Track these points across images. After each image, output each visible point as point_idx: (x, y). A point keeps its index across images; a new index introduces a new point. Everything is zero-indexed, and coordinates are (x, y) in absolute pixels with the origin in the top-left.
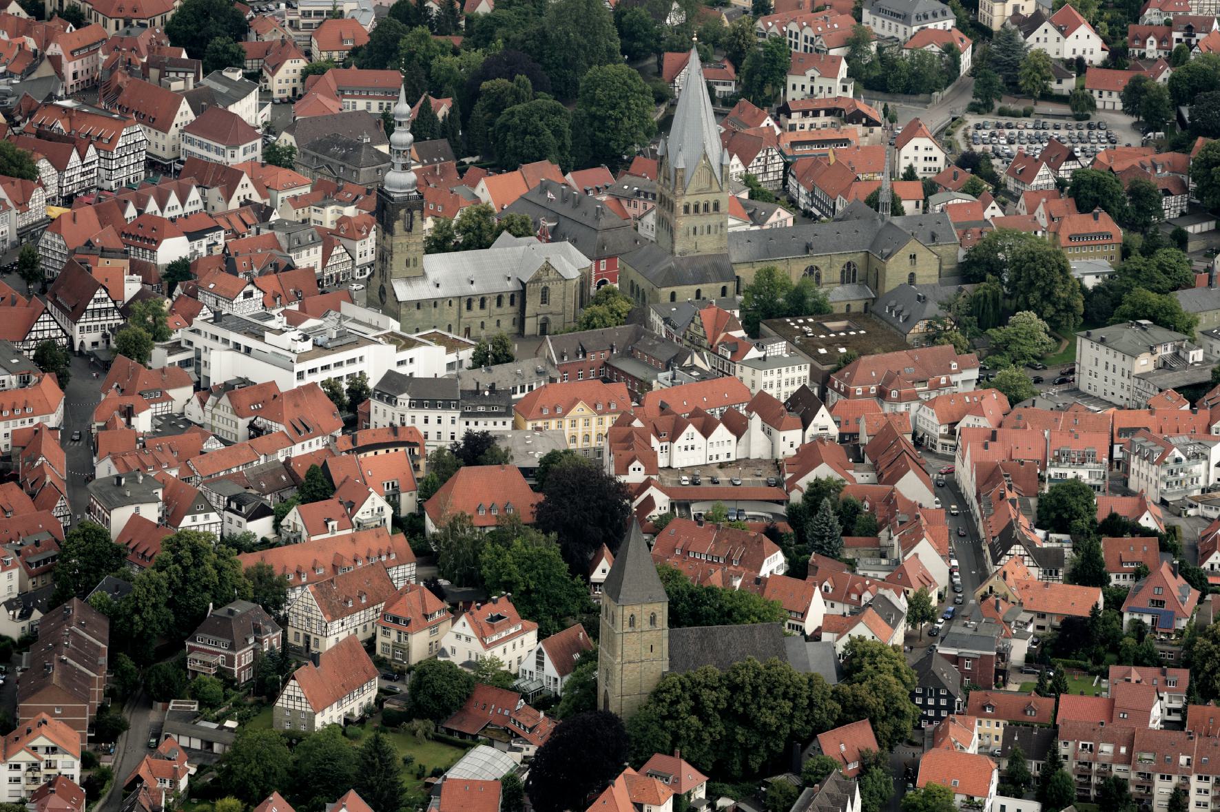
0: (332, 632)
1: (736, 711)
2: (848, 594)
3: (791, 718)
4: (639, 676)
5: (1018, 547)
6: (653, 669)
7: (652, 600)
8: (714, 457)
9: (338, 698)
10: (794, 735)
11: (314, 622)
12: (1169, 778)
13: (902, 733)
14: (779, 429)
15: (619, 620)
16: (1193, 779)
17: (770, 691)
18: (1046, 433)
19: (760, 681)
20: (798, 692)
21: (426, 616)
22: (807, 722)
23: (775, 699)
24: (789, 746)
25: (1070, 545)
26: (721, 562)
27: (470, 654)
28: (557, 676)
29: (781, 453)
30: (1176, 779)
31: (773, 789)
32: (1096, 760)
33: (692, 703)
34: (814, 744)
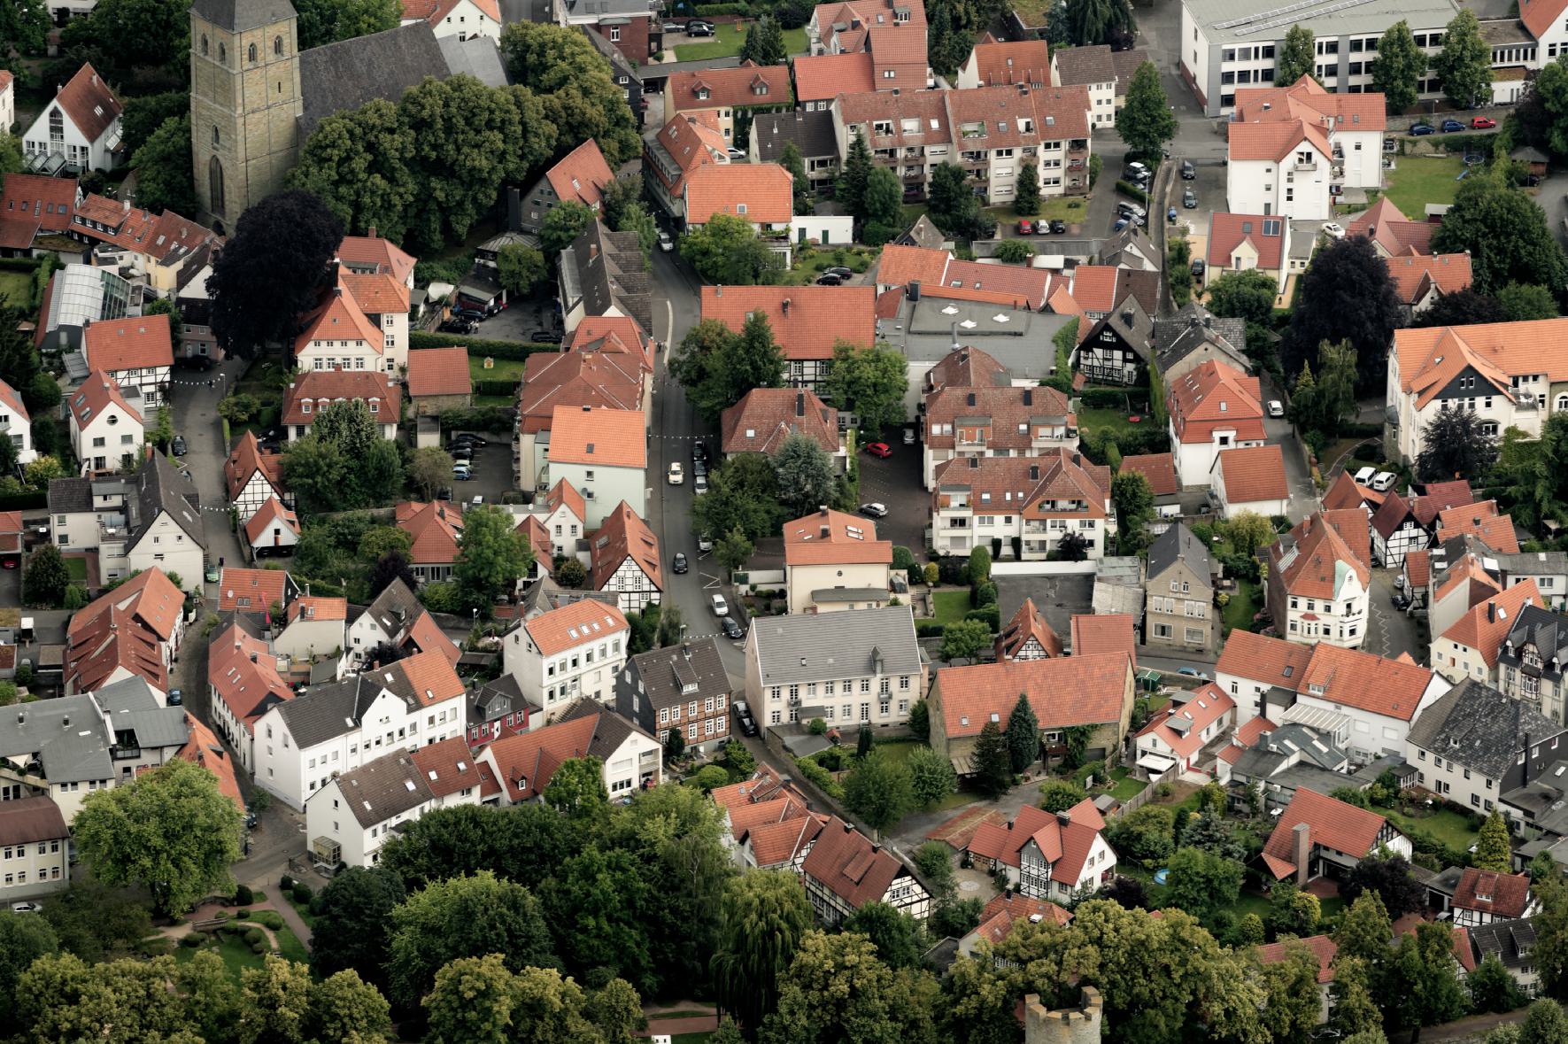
1: (426, 158)
3: (502, 157)
6: (284, 116)
7: (276, 18)
10: (508, 181)
12: (1009, 153)
16: (1041, 149)
17: (468, 122)
22: (522, 157)
23: (478, 132)
28: (85, 143)
30: (1018, 153)
31: (506, 258)
32: (901, 143)
33: (370, 157)
34: (542, 185)
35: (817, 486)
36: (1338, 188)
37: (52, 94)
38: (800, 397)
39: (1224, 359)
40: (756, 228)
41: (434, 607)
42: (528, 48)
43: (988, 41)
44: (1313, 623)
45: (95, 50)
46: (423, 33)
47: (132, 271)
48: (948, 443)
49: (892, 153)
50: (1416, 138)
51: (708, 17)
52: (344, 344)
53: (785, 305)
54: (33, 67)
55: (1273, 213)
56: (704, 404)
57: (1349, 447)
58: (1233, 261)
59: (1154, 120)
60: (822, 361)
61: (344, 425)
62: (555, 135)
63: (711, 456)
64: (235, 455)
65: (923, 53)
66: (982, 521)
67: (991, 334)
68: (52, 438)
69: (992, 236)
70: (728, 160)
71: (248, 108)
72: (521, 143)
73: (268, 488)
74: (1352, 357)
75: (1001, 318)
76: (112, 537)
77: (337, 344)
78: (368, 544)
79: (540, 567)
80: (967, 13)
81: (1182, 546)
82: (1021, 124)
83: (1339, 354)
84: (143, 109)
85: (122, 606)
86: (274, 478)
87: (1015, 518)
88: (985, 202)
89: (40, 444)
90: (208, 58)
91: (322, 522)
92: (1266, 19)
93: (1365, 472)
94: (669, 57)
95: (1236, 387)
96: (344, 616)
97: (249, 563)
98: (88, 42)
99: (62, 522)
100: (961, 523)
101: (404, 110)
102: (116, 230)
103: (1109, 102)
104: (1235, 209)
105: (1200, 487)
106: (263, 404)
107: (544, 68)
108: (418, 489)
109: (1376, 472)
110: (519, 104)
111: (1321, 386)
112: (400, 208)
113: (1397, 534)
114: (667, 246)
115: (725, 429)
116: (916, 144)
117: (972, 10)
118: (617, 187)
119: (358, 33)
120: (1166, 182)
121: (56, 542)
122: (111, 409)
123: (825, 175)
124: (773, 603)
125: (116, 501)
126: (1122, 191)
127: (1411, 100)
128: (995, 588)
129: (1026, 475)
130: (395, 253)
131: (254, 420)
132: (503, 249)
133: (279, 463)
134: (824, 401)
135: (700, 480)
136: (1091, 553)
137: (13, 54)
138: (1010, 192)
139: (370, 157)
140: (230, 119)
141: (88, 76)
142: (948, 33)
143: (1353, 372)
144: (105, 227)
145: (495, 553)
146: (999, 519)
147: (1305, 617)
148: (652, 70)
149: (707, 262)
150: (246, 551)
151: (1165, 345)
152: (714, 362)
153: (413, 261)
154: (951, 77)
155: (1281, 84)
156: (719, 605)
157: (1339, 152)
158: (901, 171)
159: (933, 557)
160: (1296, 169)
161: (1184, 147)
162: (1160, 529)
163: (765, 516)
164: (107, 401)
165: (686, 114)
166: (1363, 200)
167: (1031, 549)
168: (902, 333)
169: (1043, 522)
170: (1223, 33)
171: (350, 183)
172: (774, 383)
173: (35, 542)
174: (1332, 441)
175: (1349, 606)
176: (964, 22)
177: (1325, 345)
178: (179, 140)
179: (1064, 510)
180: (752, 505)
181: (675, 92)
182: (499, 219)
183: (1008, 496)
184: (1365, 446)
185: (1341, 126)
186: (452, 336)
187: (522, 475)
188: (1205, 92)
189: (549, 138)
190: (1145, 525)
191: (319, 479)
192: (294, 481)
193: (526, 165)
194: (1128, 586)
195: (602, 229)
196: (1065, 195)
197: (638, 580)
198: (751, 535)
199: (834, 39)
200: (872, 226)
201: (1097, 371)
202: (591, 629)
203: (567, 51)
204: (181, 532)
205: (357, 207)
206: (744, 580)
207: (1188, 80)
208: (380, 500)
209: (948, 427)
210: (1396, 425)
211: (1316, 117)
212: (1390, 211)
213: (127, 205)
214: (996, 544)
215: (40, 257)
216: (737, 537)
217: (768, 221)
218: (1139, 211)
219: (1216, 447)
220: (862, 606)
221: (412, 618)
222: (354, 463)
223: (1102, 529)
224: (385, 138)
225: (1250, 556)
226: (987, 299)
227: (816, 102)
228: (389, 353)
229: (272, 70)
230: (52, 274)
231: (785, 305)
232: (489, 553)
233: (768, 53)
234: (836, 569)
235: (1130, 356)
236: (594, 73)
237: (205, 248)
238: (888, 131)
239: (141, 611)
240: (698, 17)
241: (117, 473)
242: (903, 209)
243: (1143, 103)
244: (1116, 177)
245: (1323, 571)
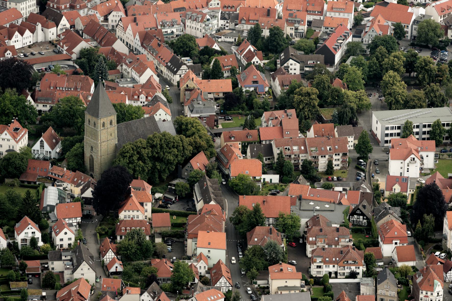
1: (155, 156)
3: (177, 156)
4: (107, 147)
5: (184, 66)
6: (112, 143)
7: (111, 114)
8: (25, 44)
10: (178, 163)
12: (325, 156)
14: (48, 28)
16: (334, 156)
17: (167, 146)
18: (155, 15)
22: (183, 156)
23: (170, 149)
24: (177, 166)
25: (192, 61)
26: (72, 89)
27: (9, 147)
28: (50, 150)
29: (49, 38)
30: (327, 157)
31: (178, 186)
33: (138, 156)
34: (189, 165)
35: (277, 255)
36: (422, 168)
37: (40, 136)
38: (271, 229)
39: (395, 219)
40: (251, 178)
41: (165, 290)
42: (182, 124)
43: (316, 123)
44: (427, 298)
45: (52, 123)
46: (152, 118)
47: (66, 189)
48: (314, 243)
49: (290, 156)
50: (442, 154)
51: (231, 115)
52: (133, 211)
53: (264, 202)
54: (32, 127)
55: (402, 175)
56: (241, 230)
57: (433, 245)
58: (393, 190)
59: (366, 147)
60: (275, 218)
61: (136, 236)
62: (192, 150)
63: (243, 245)
64: (103, 244)
65: (298, 128)
66: (326, 266)
67: (324, 211)
68: (47, 238)
69: (320, 181)
70: (242, 158)
71: (102, 141)
72: (182, 152)
73: (113, 254)
74: (433, 219)
75: (327, 206)
76: (68, 269)
77: (131, 211)
78: (144, 271)
79: (196, 279)
80: (308, 115)
81: (388, 275)
82: (328, 148)
83: (429, 218)
84: (68, 141)
85: (73, 289)
86: (115, 251)
87: (336, 266)
88: (318, 171)
89: (43, 240)
90: (90, 126)
91: (129, 264)
92: (398, 118)
93: (438, 253)
94: (220, 127)
95: (399, 228)
96: (140, 293)
97: (108, 276)
98: (50, 120)
99: (52, 263)
100: (319, 267)
101: (148, 142)
102: (62, 176)
103: (352, 142)
104: (391, 174)
105: (389, 257)
106: (109, 229)
107: (187, 130)
108: (158, 255)
109: (441, 253)
110: (182, 141)
111: (424, 228)
112: (147, 171)
113: (449, 272)
114: (224, 183)
115: (248, 238)
116: (297, 154)
117: (310, 114)
118: (210, 166)
119: (132, 119)
120: (370, 166)
121: (51, 269)
122: (65, 230)
123: (270, 162)
124: (265, 290)
125: (69, 258)
126: (357, 168)
127: (441, 142)
128: (331, 286)
129: (339, 253)
130: (146, 184)
131: (106, 233)
132: (177, 184)
133: (117, 247)
134: (276, 230)
135: (240, 253)
136: (358, 276)
137: (27, 123)
138: (325, 168)
139: (138, 156)
140: (97, 144)
141: (51, 131)
142: (303, 121)
143: (433, 223)
144: (59, 176)
145: (184, 275)
146: (331, 266)
147: (425, 296)
148: (215, 130)
149: (238, 188)
150: (107, 273)
151: (377, 215)
152: (244, 218)
153: (151, 187)
154: (304, 134)
155: (403, 137)
156: (249, 290)
157: (422, 158)
158: (293, 162)
159: (311, 277)
160: (410, 163)
161: (375, 155)
162: (378, 270)
163: (262, 264)
164: (65, 227)
165: (229, 143)
166: (429, 172)
167: (340, 275)
168: (298, 210)
169: (344, 267)
170: (386, 122)
171: (132, 163)
172: (262, 225)
173: (44, 270)
174: (426, 244)
175: (438, 293)
176: (307, 117)
177: (425, 215)
178: (80, 150)
179: (351, 264)
180: (258, 261)
181: (224, 137)
182: (175, 175)
183: (334, 259)
184: (437, 245)
185: (422, 150)
186: (163, 209)
187: (187, 251)
188: (380, 139)
189: (190, 151)
190: (374, 268)
191: (129, 252)
192: (121, 252)
193: (183, 159)
194: (370, 286)
195: (207, 178)
196: (341, 169)
197: (225, 283)
198: (258, 270)
199: (270, 122)
200: (285, 178)
201: (355, 222)
202: (214, 298)
203: (194, 125)
204: (89, 267)
205: (134, 170)
206: (256, 283)
207: (374, 136)
208: (146, 258)
209: (314, 238)
210: (446, 239)
211: (416, 147)
212: (439, 176)
213: (65, 169)
214: (330, 273)
215: (39, 184)
216: (254, 270)
217: (255, 176)
218: (363, 174)
219: (394, 246)
220: (293, 292)
221: (159, 293)
222: (139, 247)
223: (362, 269)
224: (143, 150)
225: (406, 278)
226: (321, 200)
227: (266, 141)
228: (146, 214)
229: (109, 130)
230: (43, 189)
232: (182, 275)
233: (251, 126)
234: (285, 281)
235: (365, 218)
236: (203, 131)
237: (89, 182)
238: (289, 150)
239: (79, 291)
240: (228, 115)
241: (67, 249)
242: (294, 173)
243: (363, 142)
244: (355, 164)
245: (431, 283)
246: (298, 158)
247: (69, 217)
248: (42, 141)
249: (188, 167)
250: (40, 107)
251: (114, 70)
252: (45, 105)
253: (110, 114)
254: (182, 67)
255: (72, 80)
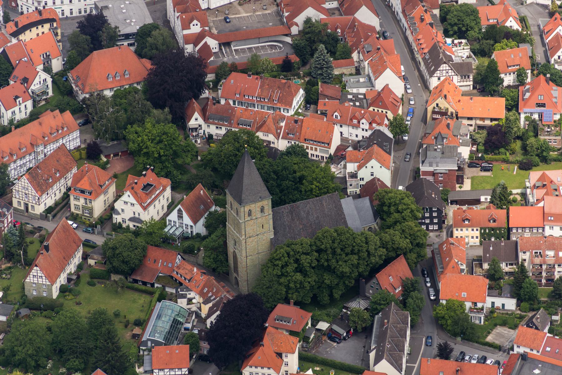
0: (42, 201)
1: (323, 265)
2: (351, 119)
3: (357, 266)
5: (444, 65)
6: (264, 238)
7: (262, 198)
9: (62, 269)
11: (30, 196)
13: (422, 257)
15: (242, 214)
19: (336, 245)
20: (360, 248)
21: (101, 186)
24: (357, 281)
25: (469, 47)
26: (266, 100)
27: (134, 213)
28: (192, 224)
32: (545, 262)
33: (296, 265)
34: (374, 281)
72: (367, 259)
90: (232, 212)
102: (189, 281)
139: (296, 265)
144: (185, 279)
149: (443, 322)
193: (369, 269)
205: (288, 288)
231: (457, 371)
246: (553, 270)
247: (170, 367)
248: (179, 210)
249: (374, 283)
250: (213, 130)
251: (348, 60)
252: (219, 126)
253: (261, 198)
254: (442, 66)
255: (268, 85)
